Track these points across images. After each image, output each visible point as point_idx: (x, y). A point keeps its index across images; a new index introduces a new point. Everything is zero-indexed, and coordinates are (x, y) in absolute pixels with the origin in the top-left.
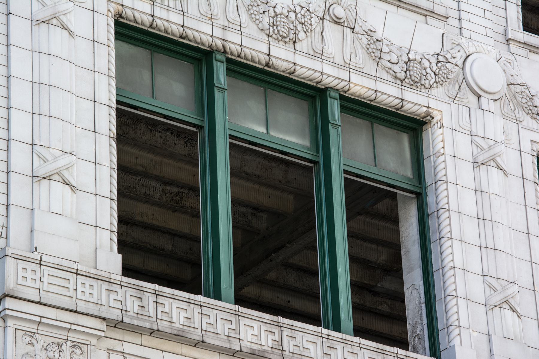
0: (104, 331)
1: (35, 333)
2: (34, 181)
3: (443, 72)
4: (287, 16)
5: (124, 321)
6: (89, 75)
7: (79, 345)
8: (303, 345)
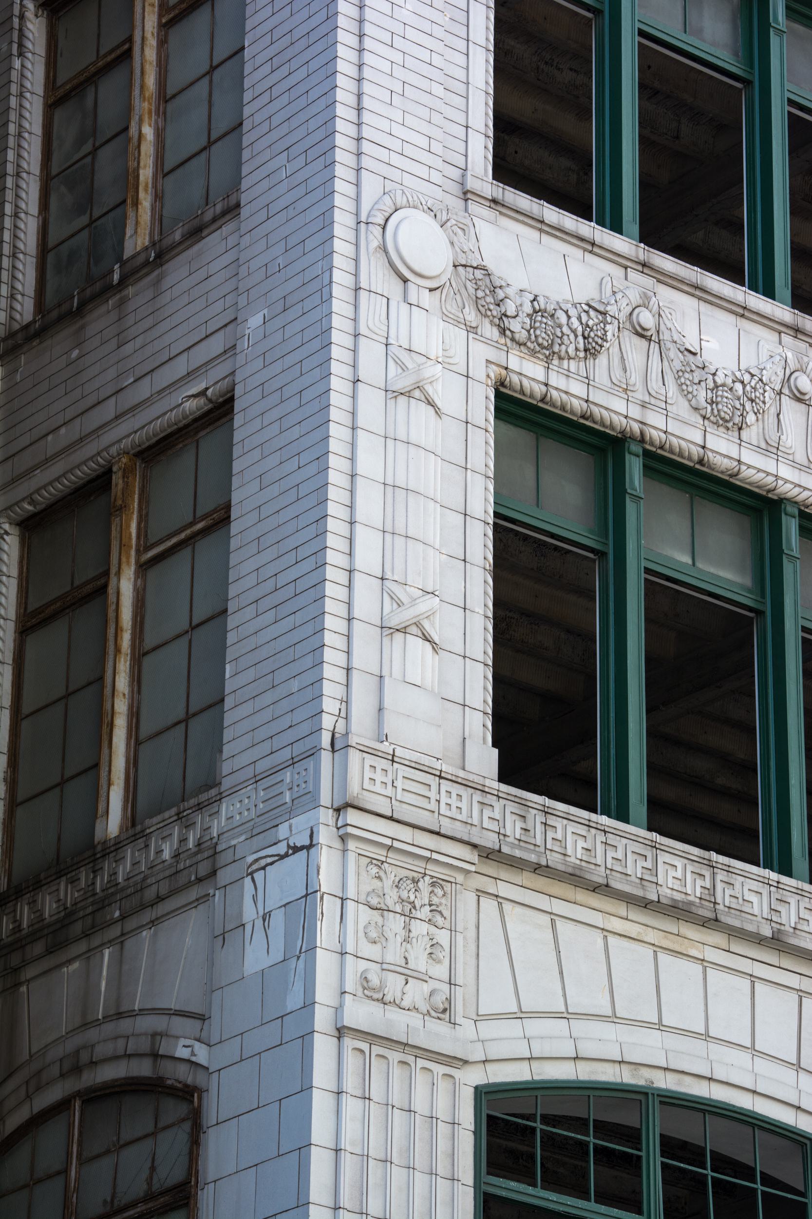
0: (474, 864)
1: (383, 862)
2: (384, 634)
3: (595, 335)
4: (731, 389)
5: (502, 851)
6: (458, 474)
7: (441, 882)
8: (743, 896)
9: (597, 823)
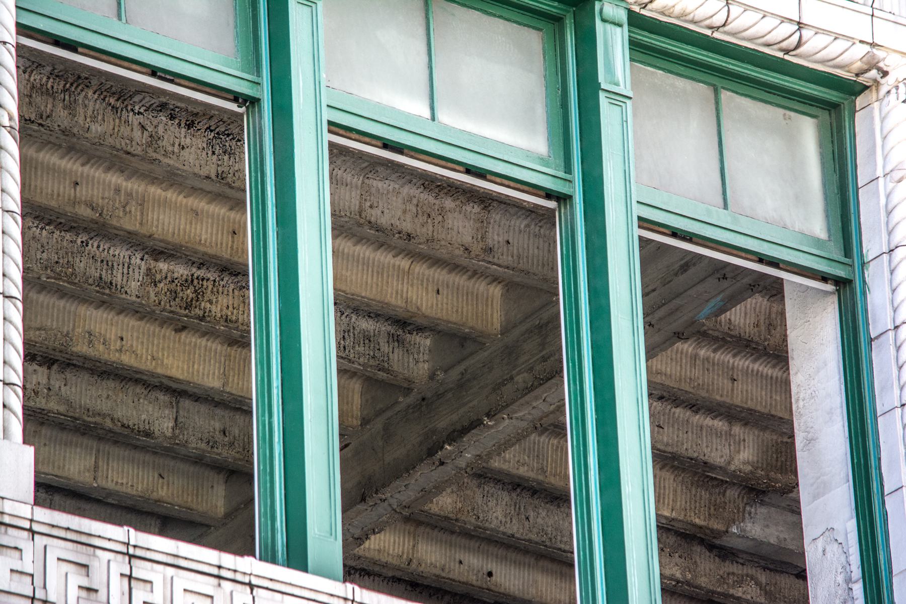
9: (235, 571)
